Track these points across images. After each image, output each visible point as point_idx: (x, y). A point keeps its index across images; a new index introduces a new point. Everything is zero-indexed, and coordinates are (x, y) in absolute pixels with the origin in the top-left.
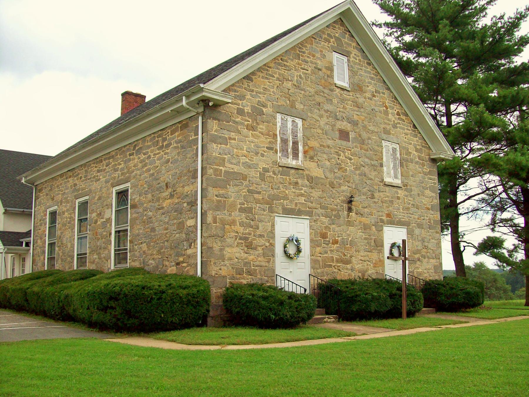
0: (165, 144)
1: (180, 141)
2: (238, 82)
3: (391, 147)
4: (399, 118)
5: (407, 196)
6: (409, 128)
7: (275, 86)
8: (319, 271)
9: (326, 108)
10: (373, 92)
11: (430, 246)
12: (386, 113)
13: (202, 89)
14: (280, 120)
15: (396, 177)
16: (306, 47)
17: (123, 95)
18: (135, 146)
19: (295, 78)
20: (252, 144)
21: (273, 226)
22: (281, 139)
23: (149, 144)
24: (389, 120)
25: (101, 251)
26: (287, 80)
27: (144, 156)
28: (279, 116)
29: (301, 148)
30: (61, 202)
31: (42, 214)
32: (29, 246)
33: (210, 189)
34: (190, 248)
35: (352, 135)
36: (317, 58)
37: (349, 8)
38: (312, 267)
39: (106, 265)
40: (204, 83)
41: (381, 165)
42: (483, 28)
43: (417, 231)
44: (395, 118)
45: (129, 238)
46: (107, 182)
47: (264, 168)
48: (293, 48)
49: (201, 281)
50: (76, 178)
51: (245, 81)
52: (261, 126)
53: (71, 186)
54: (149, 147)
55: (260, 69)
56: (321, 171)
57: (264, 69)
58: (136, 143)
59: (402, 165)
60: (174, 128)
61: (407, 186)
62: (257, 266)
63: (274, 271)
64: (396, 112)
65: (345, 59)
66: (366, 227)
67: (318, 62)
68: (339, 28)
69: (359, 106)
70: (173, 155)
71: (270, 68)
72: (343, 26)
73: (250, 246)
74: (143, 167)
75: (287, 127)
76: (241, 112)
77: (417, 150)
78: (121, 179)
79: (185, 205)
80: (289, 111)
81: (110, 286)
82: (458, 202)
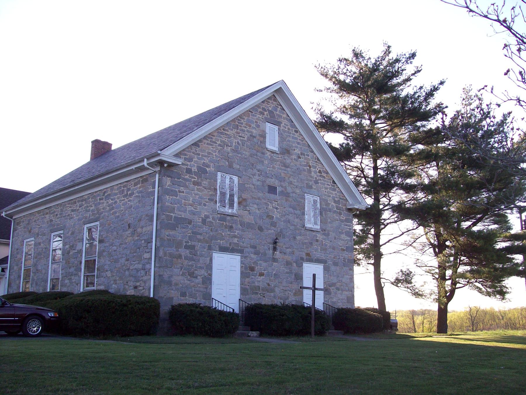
0: (129, 193)
1: (141, 192)
2: (188, 148)
3: (312, 199)
4: (320, 176)
5: (324, 239)
6: (329, 183)
7: (217, 151)
8: (247, 296)
9: (258, 168)
10: (299, 154)
11: (344, 280)
12: (310, 171)
13: (159, 155)
14: (220, 177)
15: (315, 223)
16: (244, 119)
17: (93, 142)
18: (105, 193)
19: (234, 144)
20: (197, 196)
21: (211, 260)
22: (221, 192)
23: (116, 192)
24: (311, 177)
25: (73, 277)
26: (227, 146)
27: (111, 201)
28: (219, 174)
29: (236, 199)
30: (38, 234)
31: (19, 244)
32: (4, 272)
33: (163, 231)
34: (146, 275)
35: (279, 189)
36: (253, 128)
37: (281, 88)
38: (242, 294)
39: (76, 289)
40: (161, 150)
41: (303, 214)
42: (407, 96)
43: (333, 268)
44: (317, 176)
45: (96, 267)
46: (79, 220)
47: (205, 215)
48: (233, 120)
49: (153, 300)
50: (52, 215)
51: (193, 147)
52: (205, 182)
53: (48, 222)
54: (116, 194)
55: (205, 138)
56: (252, 217)
57: (209, 138)
58: (105, 190)
59: (321, 214)
60: (136, 181)
61: (325, 231)
62: (197, 291)
63: (211, 295)
64: (318, 171)
65: (276, 128)
66: (288, 263)
67: (254, 131)
68: (272, 103)
69: (286, 166)
70: (135, 202)
71: (214, 136)
72: (276, 101)
73: (192, 275)
74: (110, 210)
75: (225, 183)
76: (189, 171)
77: (335, 202)
78: (92, 219)
79: (143, 242)
80: (229, 170)
81: (84, 301)
82: (381, 243)
